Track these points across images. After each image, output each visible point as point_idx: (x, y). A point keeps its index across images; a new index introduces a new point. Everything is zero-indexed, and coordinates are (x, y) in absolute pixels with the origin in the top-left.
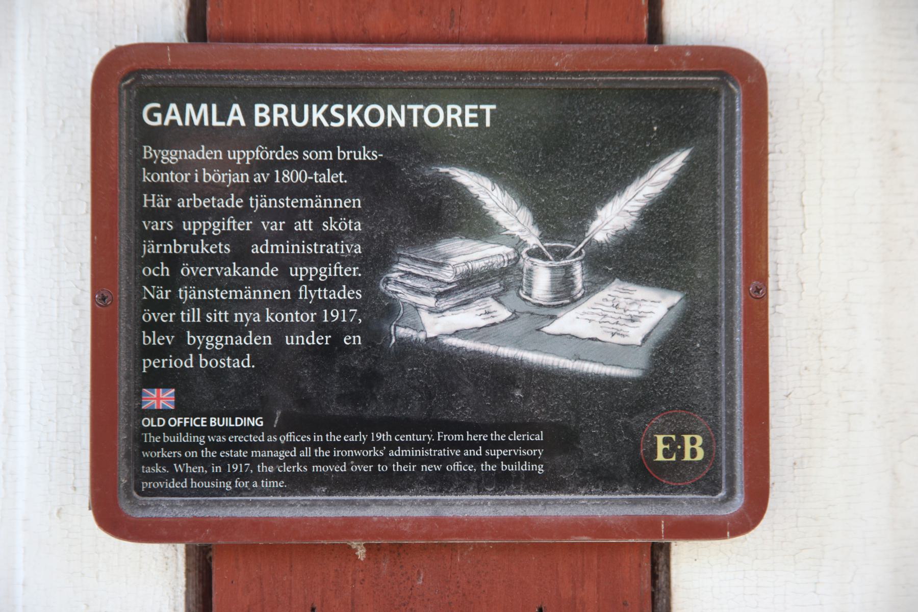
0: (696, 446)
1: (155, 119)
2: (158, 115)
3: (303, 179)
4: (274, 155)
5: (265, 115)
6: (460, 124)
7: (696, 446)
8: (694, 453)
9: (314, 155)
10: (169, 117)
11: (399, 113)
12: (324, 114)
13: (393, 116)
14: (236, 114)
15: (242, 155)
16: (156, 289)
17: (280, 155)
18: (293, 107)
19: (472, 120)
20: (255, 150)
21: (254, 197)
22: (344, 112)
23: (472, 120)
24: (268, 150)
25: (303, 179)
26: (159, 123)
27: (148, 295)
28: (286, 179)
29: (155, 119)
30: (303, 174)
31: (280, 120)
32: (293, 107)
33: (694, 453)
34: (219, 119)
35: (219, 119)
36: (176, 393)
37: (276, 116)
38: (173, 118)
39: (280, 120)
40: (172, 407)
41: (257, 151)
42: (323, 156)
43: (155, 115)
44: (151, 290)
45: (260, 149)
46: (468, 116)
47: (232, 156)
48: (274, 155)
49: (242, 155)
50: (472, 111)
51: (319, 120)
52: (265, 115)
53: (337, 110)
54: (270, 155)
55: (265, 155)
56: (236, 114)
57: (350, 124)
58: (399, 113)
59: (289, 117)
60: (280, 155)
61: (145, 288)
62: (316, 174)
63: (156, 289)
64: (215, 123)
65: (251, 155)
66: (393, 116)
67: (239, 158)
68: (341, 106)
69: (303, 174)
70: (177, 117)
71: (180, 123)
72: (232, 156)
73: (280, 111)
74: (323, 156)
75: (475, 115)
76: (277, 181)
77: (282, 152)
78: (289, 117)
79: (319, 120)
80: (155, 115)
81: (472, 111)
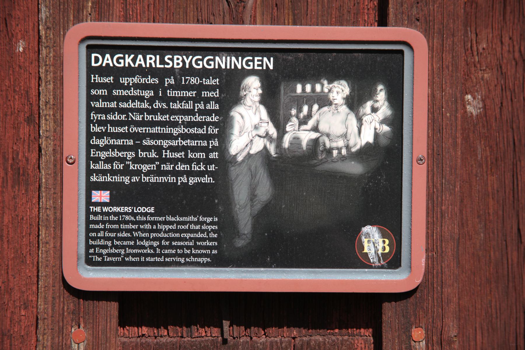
0: (386, 245)
1: (210, 65)
2: (122, 61)
3: (197, 82)
4: (145, 80)
5: (179, 61)
6: (154, 66)
7: (386, 245)
8: (384, 248)
9: (97, 92)
10: (138, 62)
11: (270, 62)
12: (132, 60)
13: (222, 62)
14: (140, 61)
15: (127, 80)
16: (136, 115)
17: (148, 81)
18: (158, 57)
19: (258, 65)
20: (134, 78)
21: (170, 90)
22: (172, 60)
23: (258, 65)
24: (142, 78)
25: (197, 82)
26: (212, 67)
27: (131, 118)
28: (192, 82)
29: (210, 65)
30: (197, 79)
31: (150, 64)
32: (158, 57)
33: (384, 248)
34: (160, 64)
35: (160, 64)
36: (110, 193)
37: (148, 61)
38: (108, 62)
39: (150, 64)
40: (108, 201)
41: (136, 78)
42: (102, 93)
43: (210, 62)
44: (133, 115)
45: (138, 77)
46: (256, 63)
47: (122, 81)
48: (145, 80)
49: (127, 80)
50: (258, 61)
51: (129, 63)
52: (179, 61)
53: (169, 59)
54: (143, 81)
55: (140, 81)
56: (140, 61)
57: (127, 65)
58: (270, 62)
59: (155, 62)
60: (148, 81)
61: (130, 114)
62: (204, 80)
63: (136, 115)
64: (158, 66)
65: (132, 80)
66: (222, 62)
67: (126, 82)
68: (171, 57)
69: (197, 79)
70: (142, 62)
71: (144, 66)
72: (122, 81)
73: (151, 59)
74: (102, 93)
75: (260, 63)
76: (183, 83)
77: (149, 79)
78: (155, 62)
79: (129, 63)
80: (210, 62)
81: (258, 61)
